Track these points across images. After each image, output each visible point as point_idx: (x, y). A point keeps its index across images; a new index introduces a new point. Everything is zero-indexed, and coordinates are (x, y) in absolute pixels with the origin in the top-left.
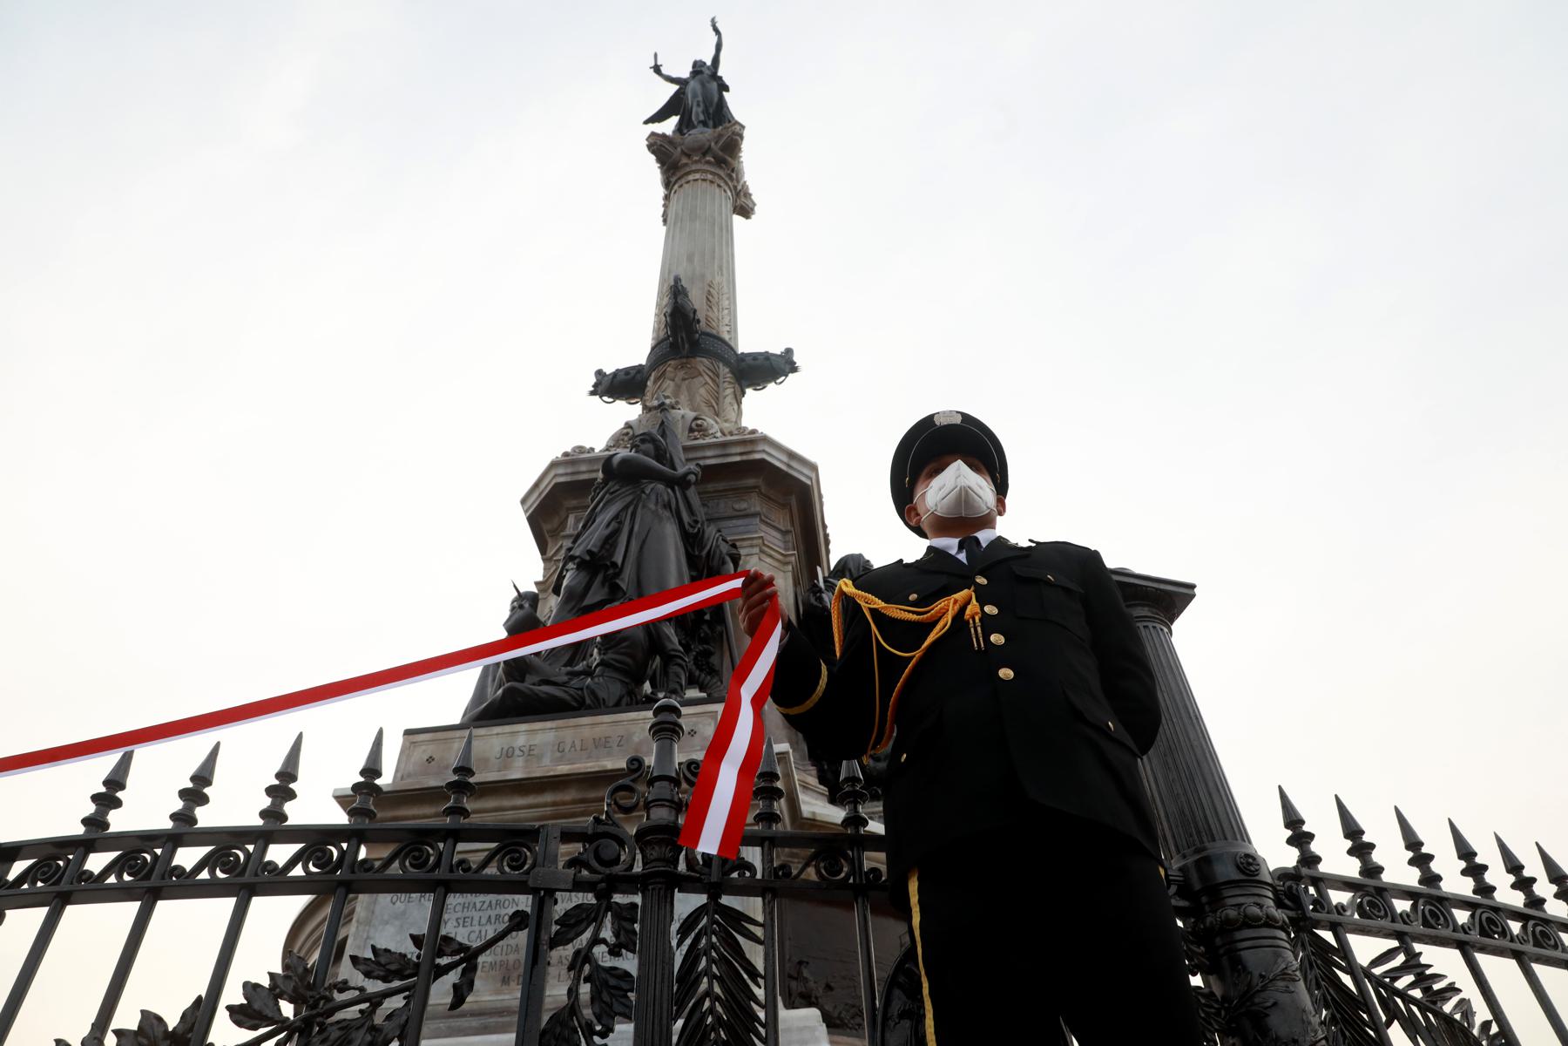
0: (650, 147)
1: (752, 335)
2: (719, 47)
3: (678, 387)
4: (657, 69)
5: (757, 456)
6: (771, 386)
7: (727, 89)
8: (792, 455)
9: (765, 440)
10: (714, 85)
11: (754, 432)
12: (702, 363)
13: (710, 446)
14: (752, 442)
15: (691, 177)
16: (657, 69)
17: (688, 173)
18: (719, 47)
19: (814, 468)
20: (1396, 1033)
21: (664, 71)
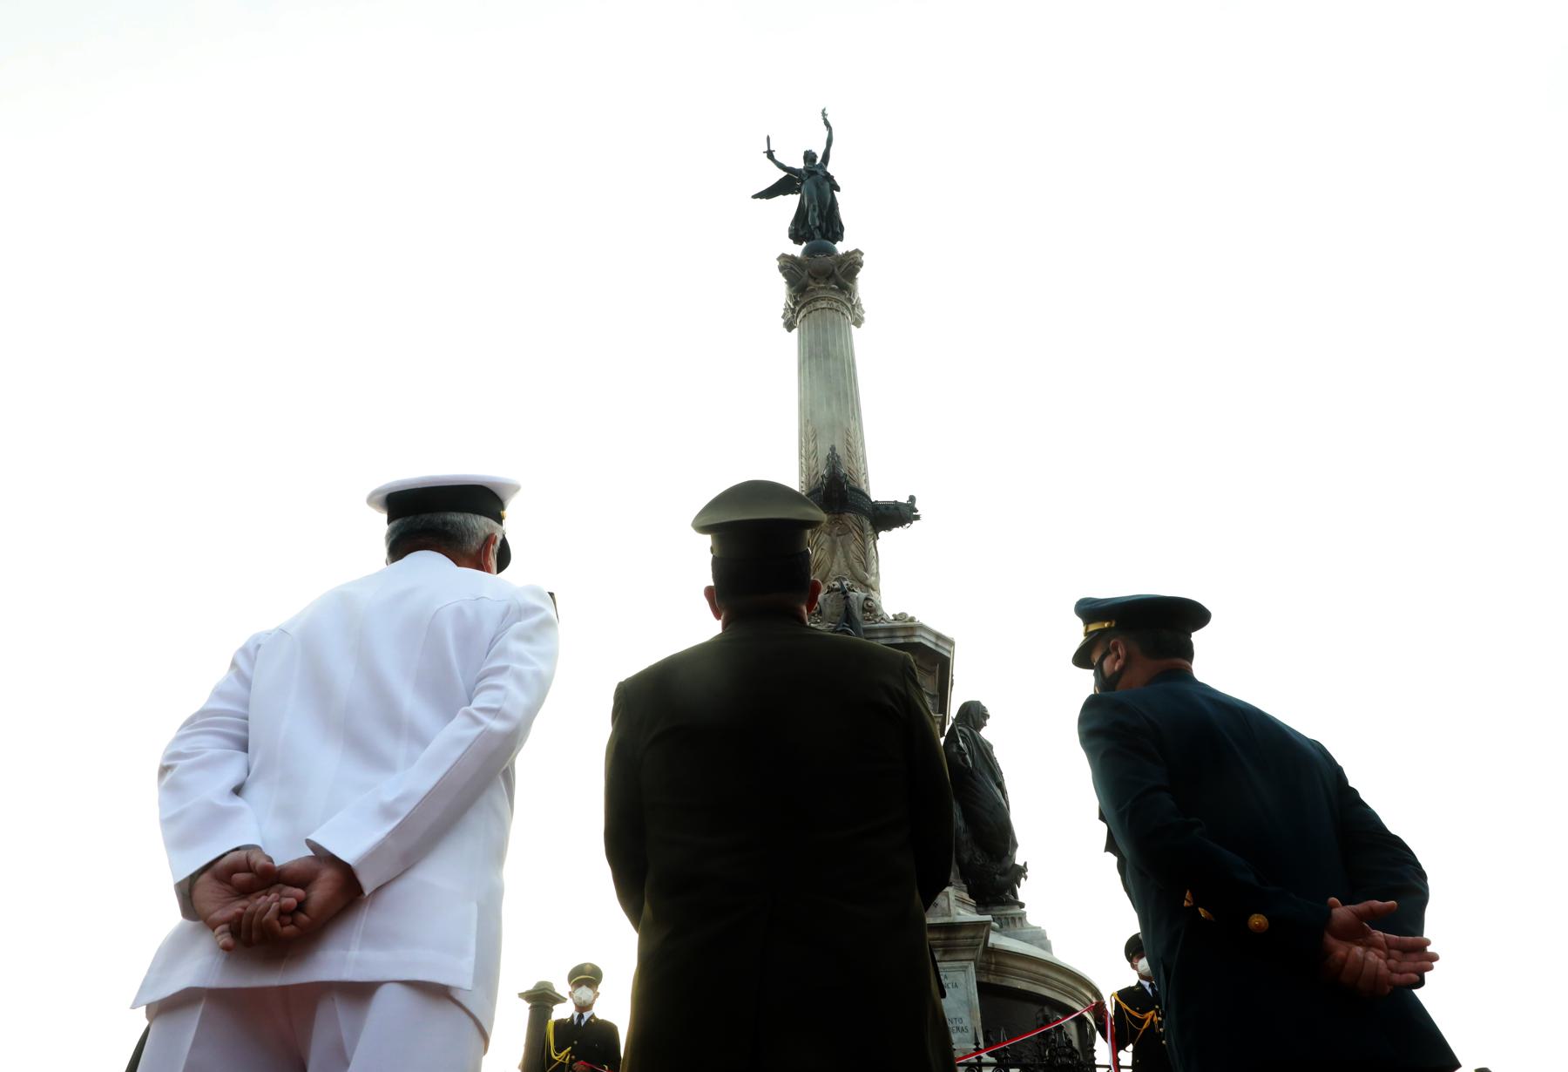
0: (781, 269)
1: (881, 488)
2: (829, 142)
3: (834, 542)
4: (770, 154)
5: (916, 640)
6: (1103, 829)
7: (838, 189)
8: (939, 636)
9: (922, 627)
10: (827, 185)
11: (912, 620)
12: (850, 518)
13: (880, 629)
14: (912, 628)
15: (819, 304)
16: (770, 154)
17: (816, 300)
18: (829, 142)
19: (952, 643)
20: (1102, 1050)
21: (777, 157)
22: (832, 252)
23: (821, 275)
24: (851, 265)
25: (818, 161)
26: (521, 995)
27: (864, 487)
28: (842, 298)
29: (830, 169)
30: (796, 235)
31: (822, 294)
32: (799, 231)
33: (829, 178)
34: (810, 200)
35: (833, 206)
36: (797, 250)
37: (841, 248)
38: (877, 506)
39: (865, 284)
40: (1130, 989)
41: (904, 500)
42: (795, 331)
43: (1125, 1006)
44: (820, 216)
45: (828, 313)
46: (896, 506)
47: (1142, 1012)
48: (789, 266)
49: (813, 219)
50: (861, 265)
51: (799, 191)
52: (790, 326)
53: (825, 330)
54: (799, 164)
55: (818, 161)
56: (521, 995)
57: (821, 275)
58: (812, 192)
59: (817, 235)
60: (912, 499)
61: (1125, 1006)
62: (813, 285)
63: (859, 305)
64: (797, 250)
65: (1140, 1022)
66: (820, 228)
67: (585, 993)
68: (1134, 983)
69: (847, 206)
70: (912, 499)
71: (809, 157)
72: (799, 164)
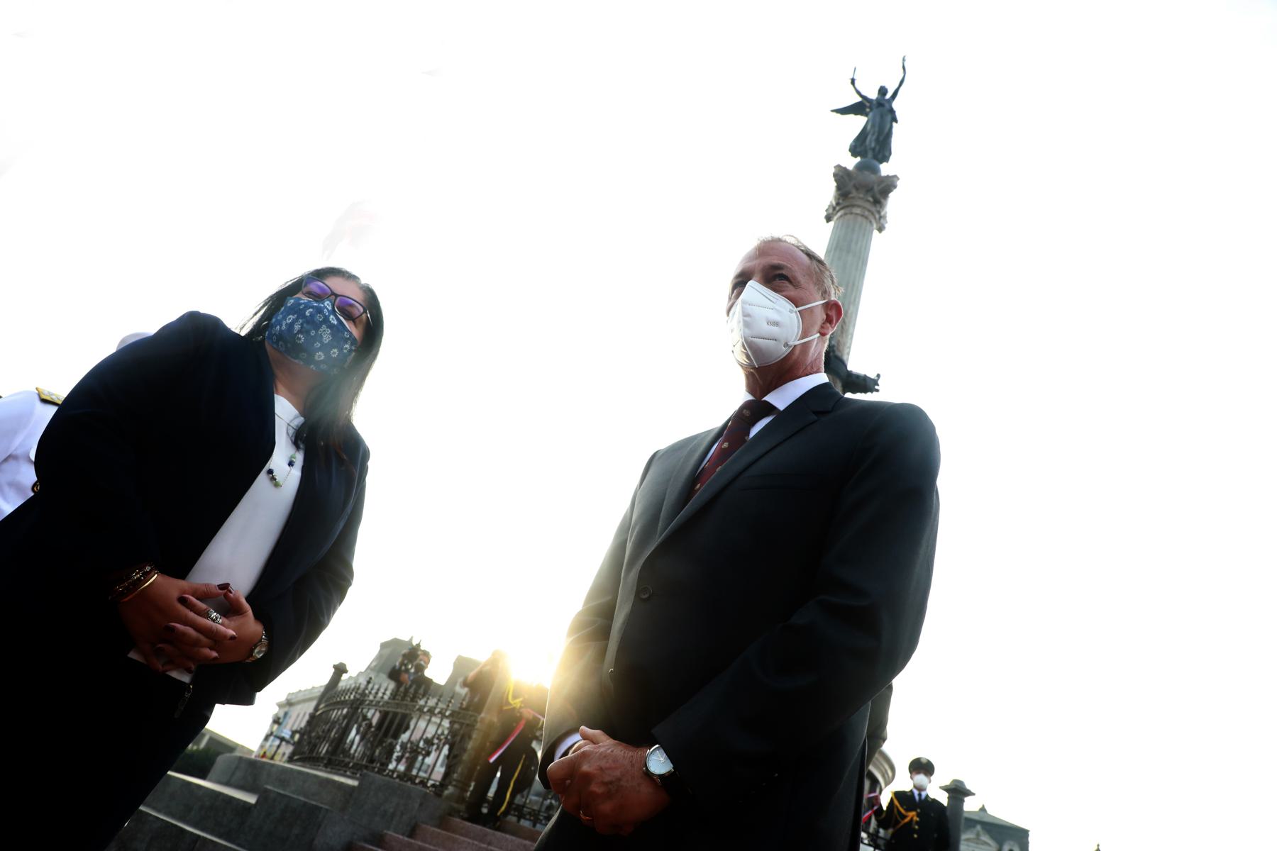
0: (835, 175)
4: (853, 82)
10: (889, 117)
15: (858, 211)
16: (853, 82)
17: (853, 206)
22: (876, 171)
23: (862, 192)
24: (888, 185)
25: (888, 96)
26: (330, 323)
27: (845, 358)
28: (873, 209)
29: (895, 105)
30: (855, 150)
31: (859, 202)
32: (858, 148)
33: (892, 112)
34: (873, 126)
35: (889, 135)
36: (851, 163)
37: (885, 169)
38: (850, 374)
39: (894, 204)
40: (904, 793)
41: (872, 376)
42: (832, 224)
43: (896, 802)
44: (877, 140)
45: (860, 219)
46: (865, 378)
47: (907, 810)
48: (842, 176)
49: (871, 141)
50: (895, 187)
51: (866, 115)
52: (828, 219)
53: (853, 230)
54: (873, 95)
55: (888, 96)
56: (330, 323)
57: (862, 192)
58: (877, 115)
59: (870, 154)
60: (878, 376)
61: (896, 802)
62: (854, 193)
63: (884, 217)
64: (851, 163)
65: (905, 817)
66: (873, 149)
67: (921, 778)
68: (908, 789)
69: (900, 136)
70: (878, 376)
71: (883, 91)
72: (873, 95)
